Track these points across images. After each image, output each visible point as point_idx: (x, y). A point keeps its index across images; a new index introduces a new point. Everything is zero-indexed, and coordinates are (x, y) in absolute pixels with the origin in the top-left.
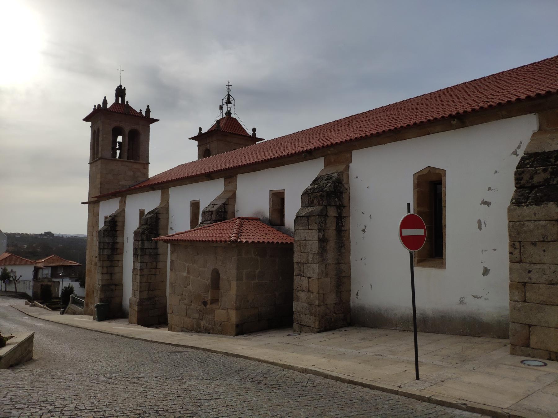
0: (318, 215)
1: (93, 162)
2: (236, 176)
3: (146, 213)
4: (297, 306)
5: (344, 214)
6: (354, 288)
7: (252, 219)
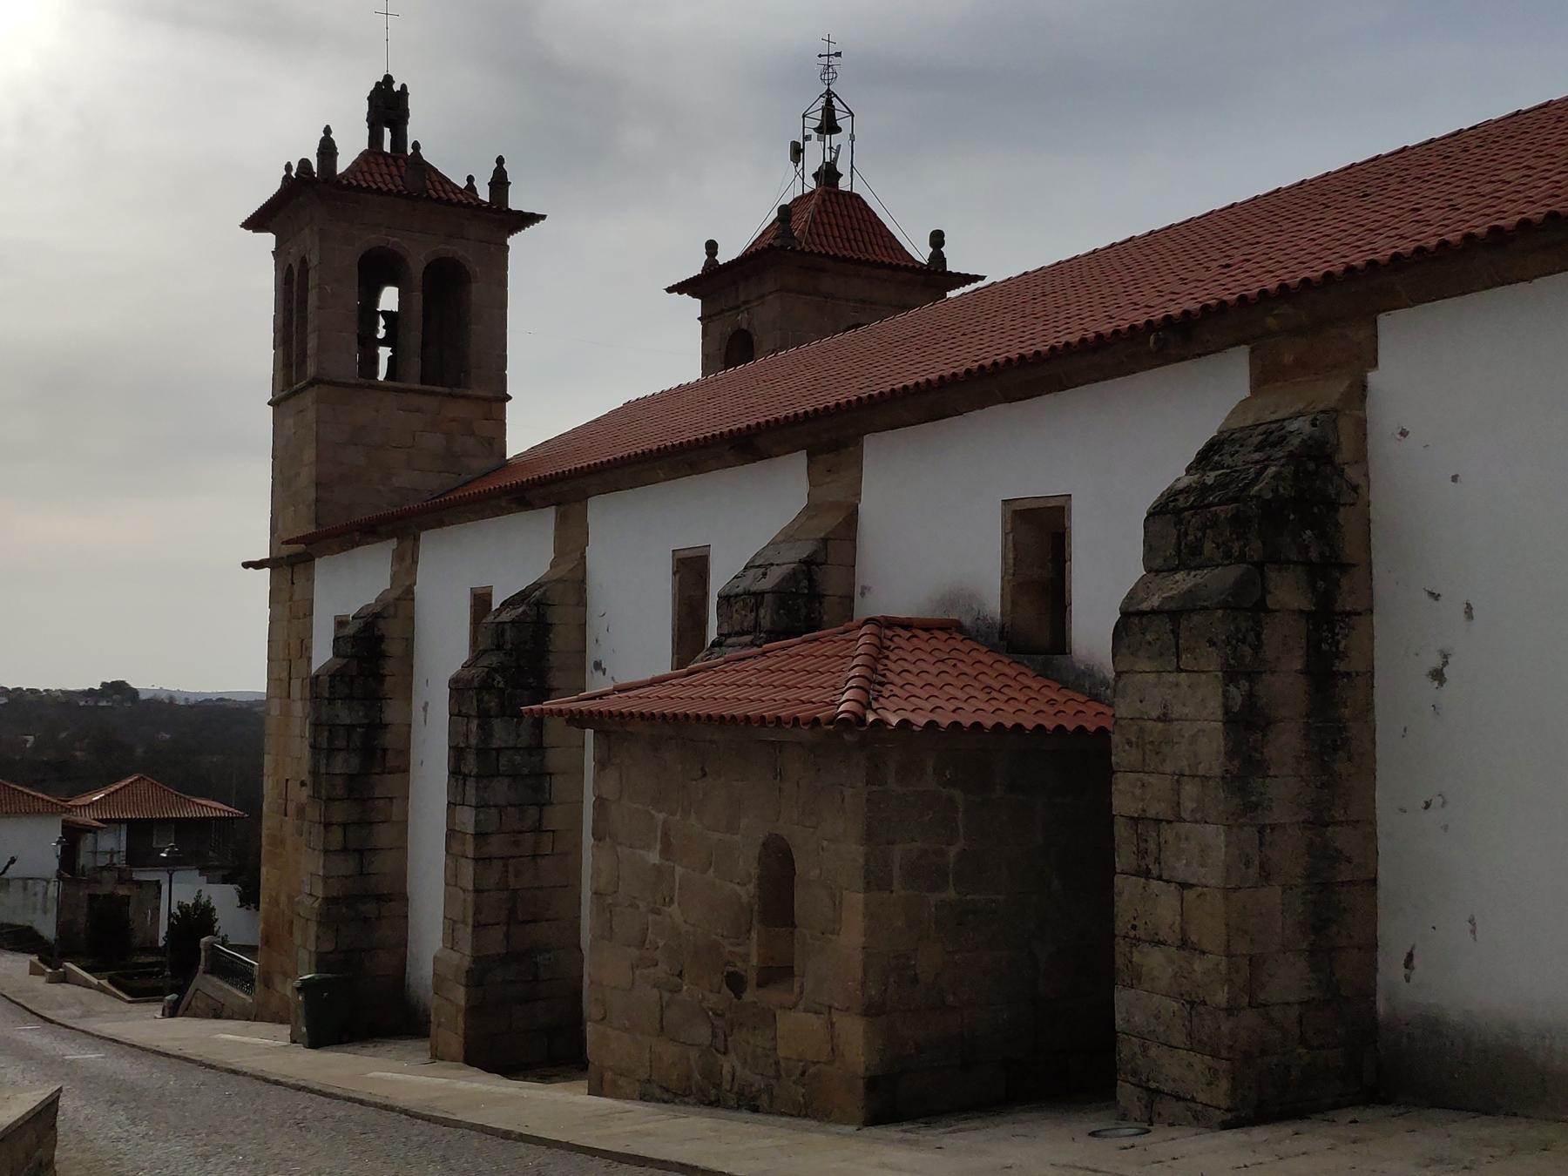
0: (1224, 606)
1: (286, 398)
2: (856, 441)
3: (495, 605)
4: (1131, 1008)
5: (1345, 602)
6: (1393, 933)
7: (928, 626)
